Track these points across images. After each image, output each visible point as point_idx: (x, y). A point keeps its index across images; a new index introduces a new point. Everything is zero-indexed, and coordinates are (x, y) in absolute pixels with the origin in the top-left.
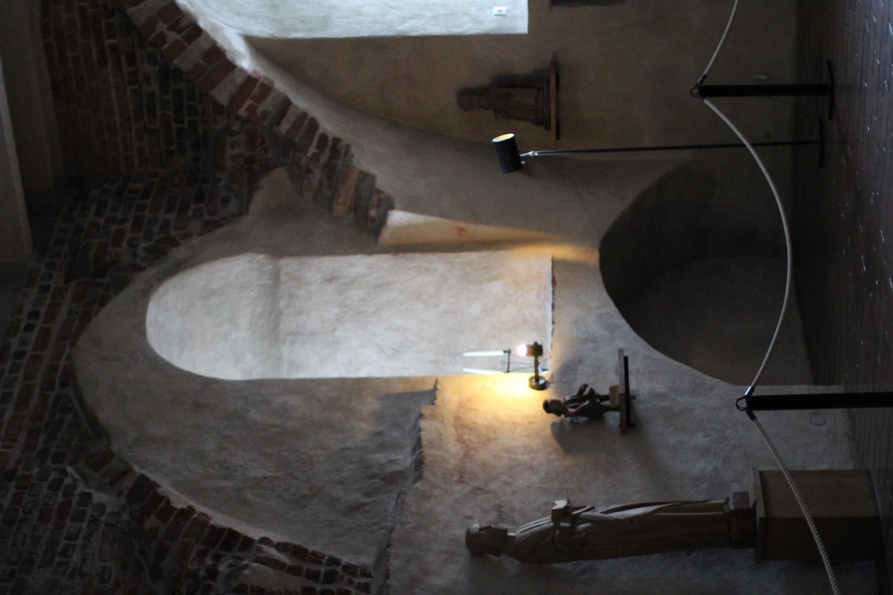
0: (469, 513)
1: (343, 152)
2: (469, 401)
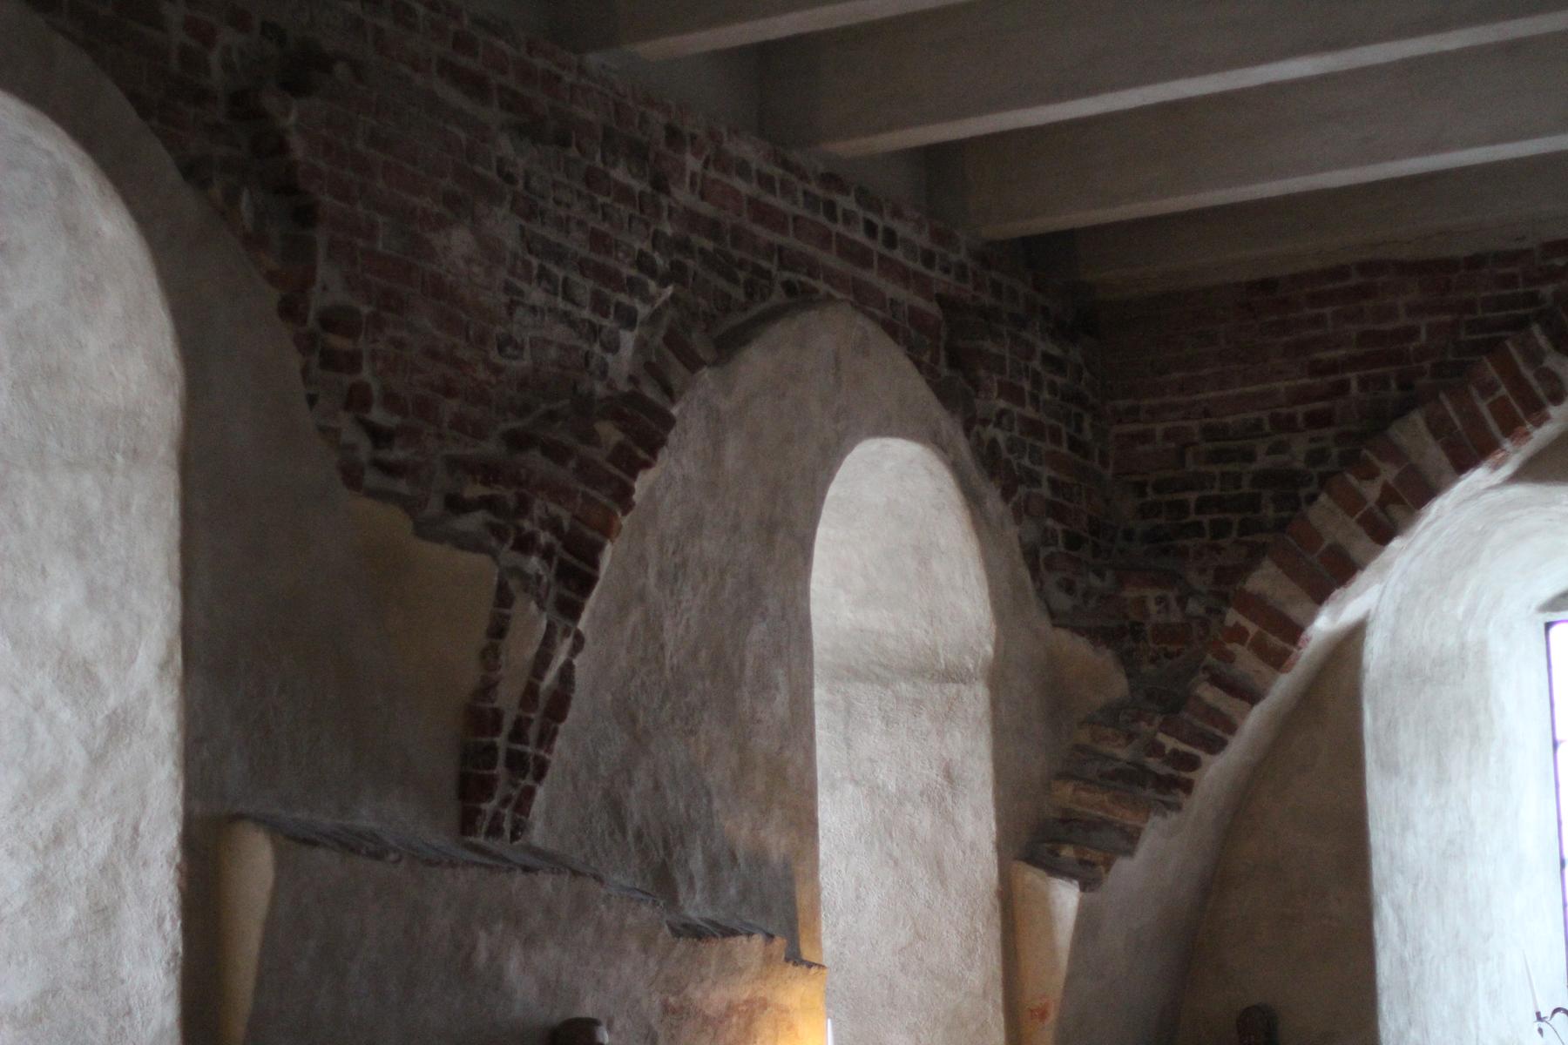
0: (617, 1025)
1: (1168, 798)
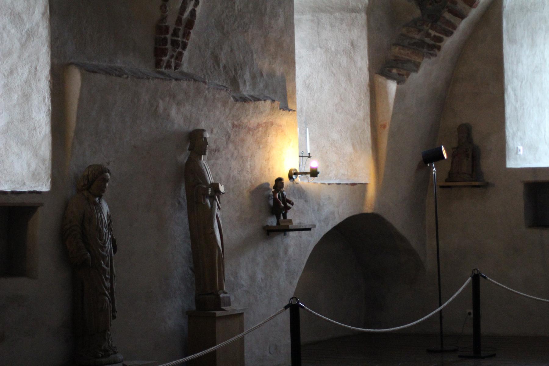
0: (215, 131)
2: (282, 131)
